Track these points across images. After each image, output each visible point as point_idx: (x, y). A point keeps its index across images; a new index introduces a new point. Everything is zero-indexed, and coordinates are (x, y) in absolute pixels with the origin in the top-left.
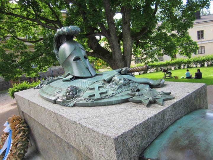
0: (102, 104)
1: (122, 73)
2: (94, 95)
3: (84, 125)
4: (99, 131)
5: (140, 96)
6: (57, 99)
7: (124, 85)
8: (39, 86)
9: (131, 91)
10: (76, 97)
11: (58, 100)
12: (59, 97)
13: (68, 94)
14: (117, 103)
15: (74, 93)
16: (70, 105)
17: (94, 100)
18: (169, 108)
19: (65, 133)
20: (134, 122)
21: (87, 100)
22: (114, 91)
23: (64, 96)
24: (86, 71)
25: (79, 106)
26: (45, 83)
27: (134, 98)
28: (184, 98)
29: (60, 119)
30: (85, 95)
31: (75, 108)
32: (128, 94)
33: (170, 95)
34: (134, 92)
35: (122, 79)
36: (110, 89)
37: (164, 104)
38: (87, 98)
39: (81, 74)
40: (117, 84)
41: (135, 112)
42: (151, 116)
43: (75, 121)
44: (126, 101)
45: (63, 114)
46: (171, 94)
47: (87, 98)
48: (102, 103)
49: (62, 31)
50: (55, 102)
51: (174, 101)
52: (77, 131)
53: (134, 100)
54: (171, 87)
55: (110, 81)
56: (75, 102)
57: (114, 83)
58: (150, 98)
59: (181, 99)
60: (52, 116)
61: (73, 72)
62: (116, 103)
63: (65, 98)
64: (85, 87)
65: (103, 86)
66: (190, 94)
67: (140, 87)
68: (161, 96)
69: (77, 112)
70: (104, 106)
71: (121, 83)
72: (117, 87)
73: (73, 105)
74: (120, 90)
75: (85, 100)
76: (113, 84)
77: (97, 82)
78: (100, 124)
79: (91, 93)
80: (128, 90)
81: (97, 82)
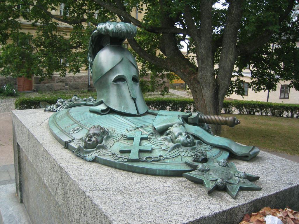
0: (137, 170)
1: (189, 121)
2: (129, 151)
3: (95, 202)
4: (113, 220)
5: (203, 171)
6: (70, 142)
7: (185, 145)
8: (53, 109)
9: (192, 158)
10: (99, 148)
11: (72, 144)
12: (74, 139)
13: (89, 140)
14: (164, 174)
15: (97, 140)
16: (87, 158)
17: (126, 160)
18: (245, 206)
19: (68, 203)
20: (175, 217)
21: (117, 156)
22: (164, 152)
23: (82, 139)
24: (131, 103)
25: (101, 164)
26: (65, 105)
27: (193, 174)
28: (277, 193)
29: (65, 179)
30: (115, 147)
31: (94, 165)
32: (187, 164)
33: (258, 181)
34: (198, 161)
35: (184, 134)
36: (160, 147)
37: (239, 197)
38: (117, 153)
39: (120, 106)
40: (172, 141)
41: (185, 199)
42: (207, 215)
43: (85, 190)
44: (177, 174)
45: (71, 173)
46: (260, 179)
47: (117, 153)
48: (139, 168)
49: (105, 28)
50: (66, 145)
51: (260, 195)
52: (85, 207)
53: (191, 177)
54: (265, 166)
55: (163, 131)
56: (97, 155)
57: (168, 137)
58: (218, 181)
59: (272, 193)
60: (55, 170)
61: (108, 101)
62: (161, 174)
63: (82, 144)
64: (121, 132)
65: (150, 138)
66: (291, 188)
67: (211, 153)
68: (239, 181)
69: (94, 173)
70: (140, 175)
71: (179, 141)
72: (171, 145)
73: (92, 159)
74: (176, 152)
75: (113, 156)
76: (165, 139)
77: (142, 127)
78: (119, 208)
79: (124, 145)
80: (189, 155)
81: (142, 127)
